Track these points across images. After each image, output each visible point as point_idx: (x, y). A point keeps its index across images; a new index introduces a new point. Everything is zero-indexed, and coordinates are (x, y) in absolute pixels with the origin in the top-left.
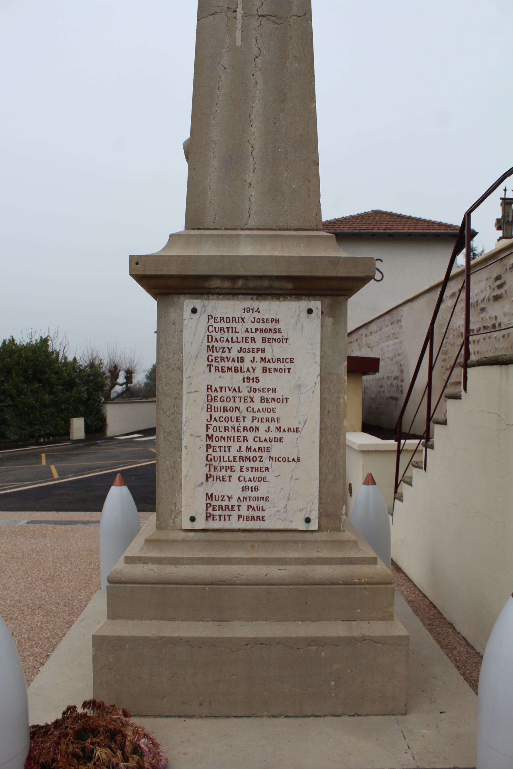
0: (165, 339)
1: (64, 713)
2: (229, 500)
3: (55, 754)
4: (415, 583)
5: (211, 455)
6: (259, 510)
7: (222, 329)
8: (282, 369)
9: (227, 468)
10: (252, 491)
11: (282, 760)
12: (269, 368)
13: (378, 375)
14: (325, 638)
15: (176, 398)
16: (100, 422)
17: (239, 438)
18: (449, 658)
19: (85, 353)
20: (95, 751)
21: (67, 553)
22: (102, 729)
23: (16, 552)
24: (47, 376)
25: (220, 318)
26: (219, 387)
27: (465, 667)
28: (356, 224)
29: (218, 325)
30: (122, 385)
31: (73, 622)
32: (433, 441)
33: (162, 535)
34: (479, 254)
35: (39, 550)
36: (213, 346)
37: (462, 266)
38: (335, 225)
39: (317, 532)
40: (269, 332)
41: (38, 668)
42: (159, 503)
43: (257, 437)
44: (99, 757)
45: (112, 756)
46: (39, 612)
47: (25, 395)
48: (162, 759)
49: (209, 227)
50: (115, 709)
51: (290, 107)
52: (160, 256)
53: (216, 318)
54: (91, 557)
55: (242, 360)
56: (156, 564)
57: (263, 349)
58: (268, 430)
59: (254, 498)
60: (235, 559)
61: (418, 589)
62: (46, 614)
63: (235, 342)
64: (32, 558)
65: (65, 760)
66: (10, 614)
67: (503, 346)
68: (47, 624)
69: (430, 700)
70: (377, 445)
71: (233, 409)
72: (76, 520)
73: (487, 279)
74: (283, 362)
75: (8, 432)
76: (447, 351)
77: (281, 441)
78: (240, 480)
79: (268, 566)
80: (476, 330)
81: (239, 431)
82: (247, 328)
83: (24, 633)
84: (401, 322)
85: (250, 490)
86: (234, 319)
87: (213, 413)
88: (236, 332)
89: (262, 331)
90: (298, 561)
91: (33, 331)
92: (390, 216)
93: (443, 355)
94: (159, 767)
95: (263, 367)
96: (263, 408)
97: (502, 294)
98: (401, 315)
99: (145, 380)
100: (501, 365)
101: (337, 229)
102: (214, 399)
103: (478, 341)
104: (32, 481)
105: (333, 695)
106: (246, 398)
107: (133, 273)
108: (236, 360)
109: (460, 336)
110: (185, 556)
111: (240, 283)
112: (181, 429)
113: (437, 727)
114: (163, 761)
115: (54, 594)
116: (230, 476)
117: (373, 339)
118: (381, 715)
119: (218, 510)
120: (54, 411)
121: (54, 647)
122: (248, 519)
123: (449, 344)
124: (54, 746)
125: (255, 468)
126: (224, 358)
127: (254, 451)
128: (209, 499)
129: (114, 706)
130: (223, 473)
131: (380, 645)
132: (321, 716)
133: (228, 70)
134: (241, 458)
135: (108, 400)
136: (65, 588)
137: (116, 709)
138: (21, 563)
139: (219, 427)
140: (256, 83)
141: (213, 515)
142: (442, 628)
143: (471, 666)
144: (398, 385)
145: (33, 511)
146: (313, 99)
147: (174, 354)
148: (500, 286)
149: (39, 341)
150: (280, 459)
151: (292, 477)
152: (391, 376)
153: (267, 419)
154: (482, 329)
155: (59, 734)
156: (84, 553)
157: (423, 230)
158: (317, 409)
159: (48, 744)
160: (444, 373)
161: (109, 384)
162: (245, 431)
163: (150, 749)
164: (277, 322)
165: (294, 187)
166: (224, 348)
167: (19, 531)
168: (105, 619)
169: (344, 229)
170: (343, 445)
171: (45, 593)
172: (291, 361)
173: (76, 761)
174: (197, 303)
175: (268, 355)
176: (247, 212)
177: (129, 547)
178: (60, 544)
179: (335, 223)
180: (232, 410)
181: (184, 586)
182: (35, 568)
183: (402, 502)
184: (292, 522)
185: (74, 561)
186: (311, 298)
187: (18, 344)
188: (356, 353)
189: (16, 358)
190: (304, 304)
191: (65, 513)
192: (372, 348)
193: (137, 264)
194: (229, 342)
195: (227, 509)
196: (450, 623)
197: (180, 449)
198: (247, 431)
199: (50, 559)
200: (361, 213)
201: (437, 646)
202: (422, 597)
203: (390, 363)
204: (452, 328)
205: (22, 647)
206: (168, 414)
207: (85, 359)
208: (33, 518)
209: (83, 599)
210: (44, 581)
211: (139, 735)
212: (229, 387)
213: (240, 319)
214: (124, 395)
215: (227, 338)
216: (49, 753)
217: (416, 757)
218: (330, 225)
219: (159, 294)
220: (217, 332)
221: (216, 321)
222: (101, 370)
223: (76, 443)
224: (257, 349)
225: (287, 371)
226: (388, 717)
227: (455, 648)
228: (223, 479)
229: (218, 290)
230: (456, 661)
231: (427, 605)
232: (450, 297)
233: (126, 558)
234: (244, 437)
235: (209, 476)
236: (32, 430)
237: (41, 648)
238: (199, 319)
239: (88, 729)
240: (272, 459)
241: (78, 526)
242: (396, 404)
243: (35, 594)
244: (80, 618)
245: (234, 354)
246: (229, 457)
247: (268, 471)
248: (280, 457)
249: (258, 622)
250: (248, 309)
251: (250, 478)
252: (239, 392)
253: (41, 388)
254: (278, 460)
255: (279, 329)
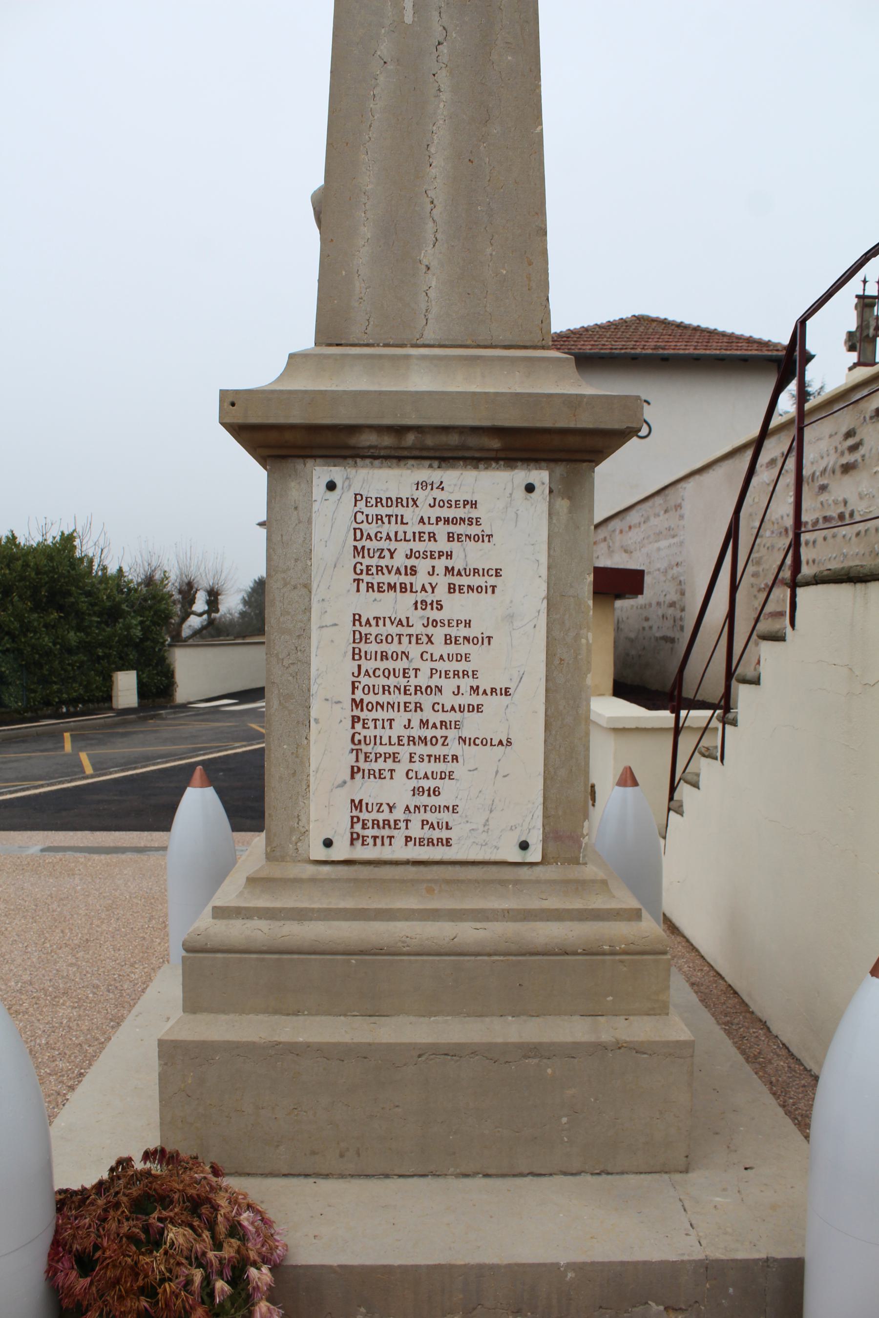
0: (282, 535)
1: (112, 1170)
2: (391, 811)
3: (99, 1236)
4: (703, 953)
5: (360, 734)
6: (440, 827)
7: (379, 517)
8: (481, 587)
9: (387, 755)
10: (429, 795)
11: (479, 1247)
12: (460, 586)
13: (640, 600)
14: (552, 1044)
15: (299, 636)
16: (164, 679)
17: (407, 705)
18: (760, 1078)
19: (137, 560)
20: (166, 1232)
21: (110, 902)
22: (176, 1196)
23: (23, 899)
24: (73, 600)
25: (376, 498)
26: (374, 618)
27: (786, 1094)
28: (605, 339)
29: (372, 511)
30: (200, 615)
31: (122, 1018)
32: (737, 712)
33: (276, 871)
34: (816, 393)
35: (62, 896)
36: (363, 548)
37: (786, 413)
38: (569, 341)
39: (541, 866)
40: (460, 524)
41: (65, 1095)
42: (270, 815)
43: (438, 704)
44: (173, 1242)
45: (195, 1239)
46: (64, 1001)
47: (35, 632)
48: (277, 1246)
49: (357, 342)
50: (197, 1163)
51: (498, 133)
52: (273, 392)
53: (369, 500)
54: (152, 908)
55: (413, 571)
56: (266, 919)
57: (449, 553)
58: (458, 692)
59: (433, 808)
60: (400, 910)
61: (708, 963)
62: (76, 1005)
63: (401, 540)
64: (51, 910)
65: (116, 1247)
66: (14, 1004)
67: (857, 550)
68: (79, 1022)
69: (728, 1147)
70: (639, 718)
71: (397, 655)
72: (125, 845)
73: (831, 436)
74: (483, 575)
75: (7, 695)
76: (761, 558)
77: (480, 710)
78: (410, 777)
79: (457, 923)
80: (810, 523)
81: (408, 692)
82: (422, 517)
83: (40, 1037)
84: (681, 508)
85: (426, 793)
86: (399, 500)
87: (363, 662)
88: (402, 523)
89: (447, 521)
90: (506, 914)
91: (49, 521)
92: (664, 325)
93: (753, 565)
94: (273, 1258)
95: (449, 584)
96: (449, 654)
97: (856, 461)
98: (683, 496)
99: (241, 607)
100: (855, 583)
101: (573, 347)
102: (365, 638)
103: (814, 542)
104: (48, 780)
105: (566, 1139)
106: (419, 637)
107: (225, 421)
108: (403, 571)
109: (784, 533)
110: (316, 906)
111: (410, 439)
112: (309, 690)
113: (739, 1192)
114: (280, 1248)
115: (90, 971)
116: (392, 771)
117: (633, 538)
118: (645, 1173)
119: (371, 827)
120: (85, 659)
121: (91, 1060)
122: (422, 844)
123: (764, 546)
124: (97, 1224)
125: (435, 756)
126: (382, 567)
127: (432, 727)
128: (356, 808)
129: (196, 1158)
130: (380, 764)
131: (645, 1056)
132: (544, 1175)
133: (390, 67)
134: (411, 739)
135: (178, 640)
136: (108, 960)
137: (199, 1163)
138: (33, 918)
139: (374, 686)
140: (439, 90)
141: (363, 837)
142: (748, 1028)
143: (795, 1092)
144: (674, 617)
145: (52, 830)
146: (538, 118)
147: (296, 560)
148: (853, 448)
149: (58, 538)
150: (478, 742)
151: (497, 772)
152: (664, 602)
153: (456, 672)
154: (821, 521)
155: (106, 1204)
156: (139, 902)
157: (720, 349)
158: (542, 656)
159: (87, 1220)
160: (755, 596)
161: (179, 613)
162: (419, 692)
163: (257, 1229)
164: (474, 506)
165: (504, 272)
166: (383, 550)
167: (28, 864)
168: (178, 1013)
169: (584, 347)
170: (584, 719)
171: (74, 969)
172: (498, 573)
173: (134, 1248)
174: (336, 473)
175: (457, 563)
176: (423, 317)
177: (220, 891)
178: (98, 886)
179: (568, 337)
180: (395, 656)
181: (313, 957)
182: (56, 926)
183: (682, 815)
184: (497, 848)
185: (123, 915)
186: (532, 465)
187: (22, 544)
188: (605, 562)
189: (19, 569)
190: (521, 476)
191: (105, 833)
192: (631, 552)
193: (233, 404)
194: (391, 540)
195: (386, 827)
196: (761, 1021)
197: (307, 722)
198: (422, 693)
199: (81, 912)
200: (615, 321)
201: (740, 1058)
202: (715, 976)
203: (663, 578)
204: (769, 520)
205: (37, 1060)
206: (286, 663)
207: (138, 570)
208: (52, 843)
209: (140, 980)
210: (72, 949)
211: (239, 1206)
212: (390, 618)
213: (410, 501)
214: (204, 632)
215: (388, 534)
216: (88, 1235)
217: (703, 1242)
218: (564, 340)
219: (270, 456)
220: (369, 524)
221: (369, 504)
222: (165, 590)
223: (124, 715)
224: (439, 552)
225: (490, 590)
226: (656, 1176)
227: (770, 1062)
228: (380, 774)
229: (372, 451)
230: (771, 1083)
231: (722, 990)
232: (767, 467)
233: (215, 908)
234: (416, 703)
235: (356, 769)
236: (48, 691)
237: (69, 1062)
238: (339, 500)
239: (154, 1196)
240: (465, 741)
241: (129, 856)
242: (672, 649)
243: (57, 970)
244: (134, 1011)
245: (400, 561)
246: (390, 737)
247: (457, 762)
248: (478, 738)
249: (439, 1019)
250: (424, 484)
251: (426, 773)
252: (408, 625)
253: (62, 620)
254: (473, 742)
255: (477, 518)
